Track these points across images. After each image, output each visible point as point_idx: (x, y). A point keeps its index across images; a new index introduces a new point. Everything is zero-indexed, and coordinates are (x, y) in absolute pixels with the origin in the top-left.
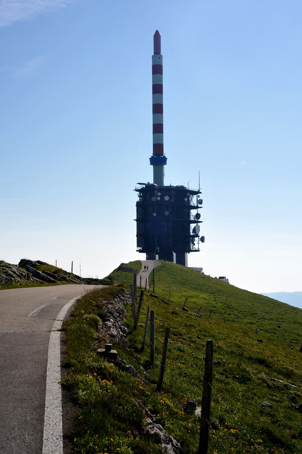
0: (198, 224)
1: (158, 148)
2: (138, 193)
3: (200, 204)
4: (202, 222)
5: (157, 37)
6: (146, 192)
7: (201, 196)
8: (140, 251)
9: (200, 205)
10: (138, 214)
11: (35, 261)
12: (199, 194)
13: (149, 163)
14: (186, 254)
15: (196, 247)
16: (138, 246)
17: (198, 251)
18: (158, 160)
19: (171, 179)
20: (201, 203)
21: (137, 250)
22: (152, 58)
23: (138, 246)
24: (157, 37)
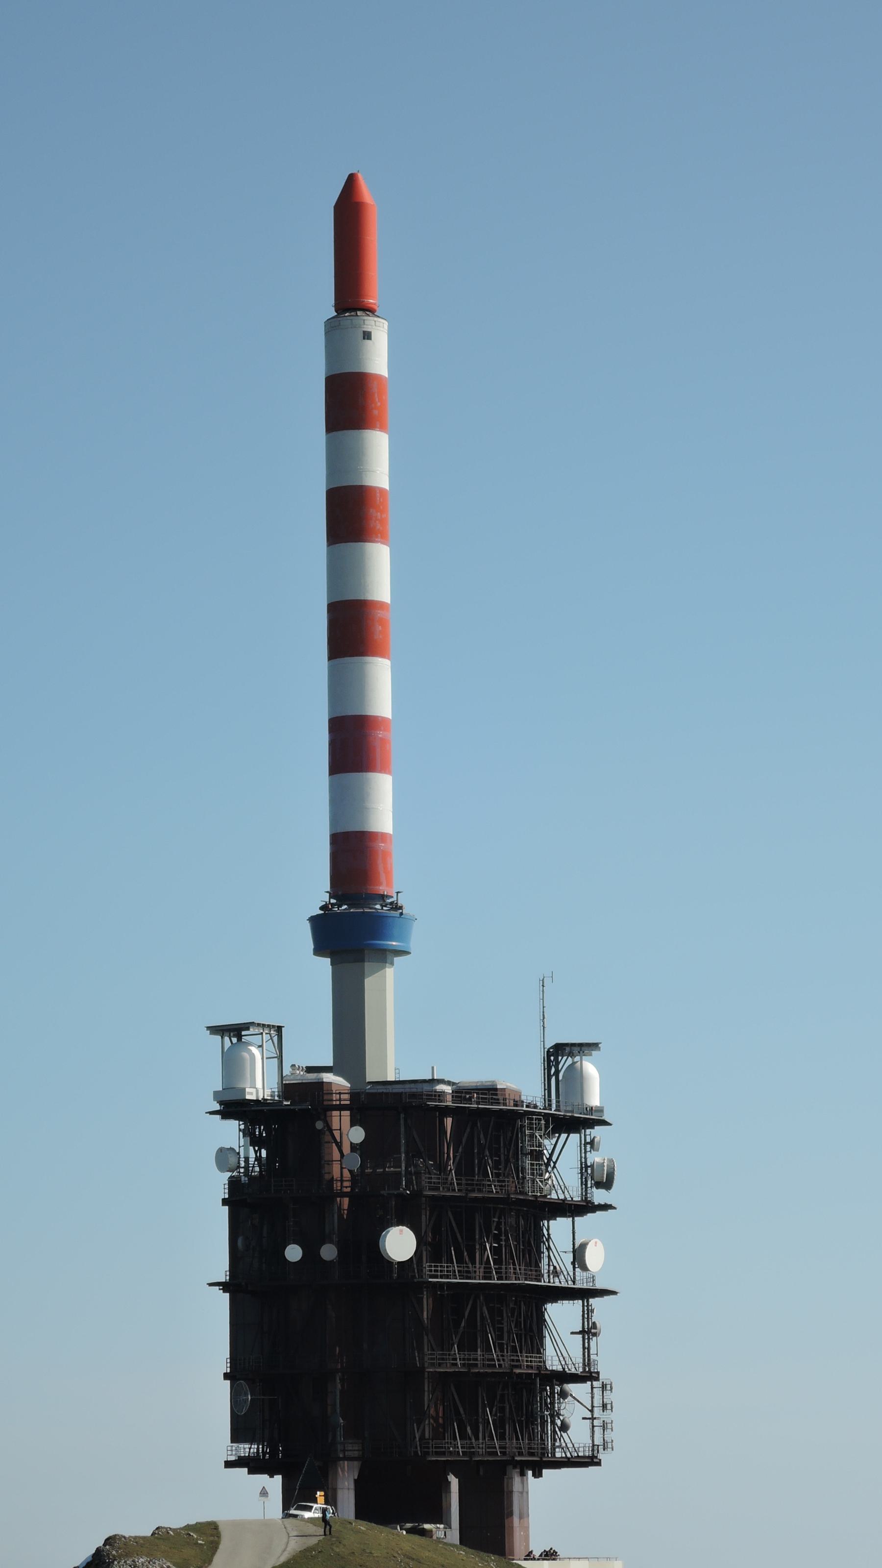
0: (591, 1301)
1: (353, 856)
2: (231, 1133)
3: (599, 1185)
4: (614, 1293)
5: (349, 214)
6: (283, 1131)
7: (608, 1147)
8: (254, 1465)
9: (599, 1196)
10: (408, 1086)
11: (180, 1529)
12: (597, 1132)
13: (310, 945)
14: (517, 1480)
15: (578, 1438)
16: (238, 1435)
17: (592, 1461)
18: (354, 925)
19: (435, 1030)
20: (606, 1184)
21: (233, 1458)
22: (327, 333)
23: (236, 1436)
24: (349, 214)
